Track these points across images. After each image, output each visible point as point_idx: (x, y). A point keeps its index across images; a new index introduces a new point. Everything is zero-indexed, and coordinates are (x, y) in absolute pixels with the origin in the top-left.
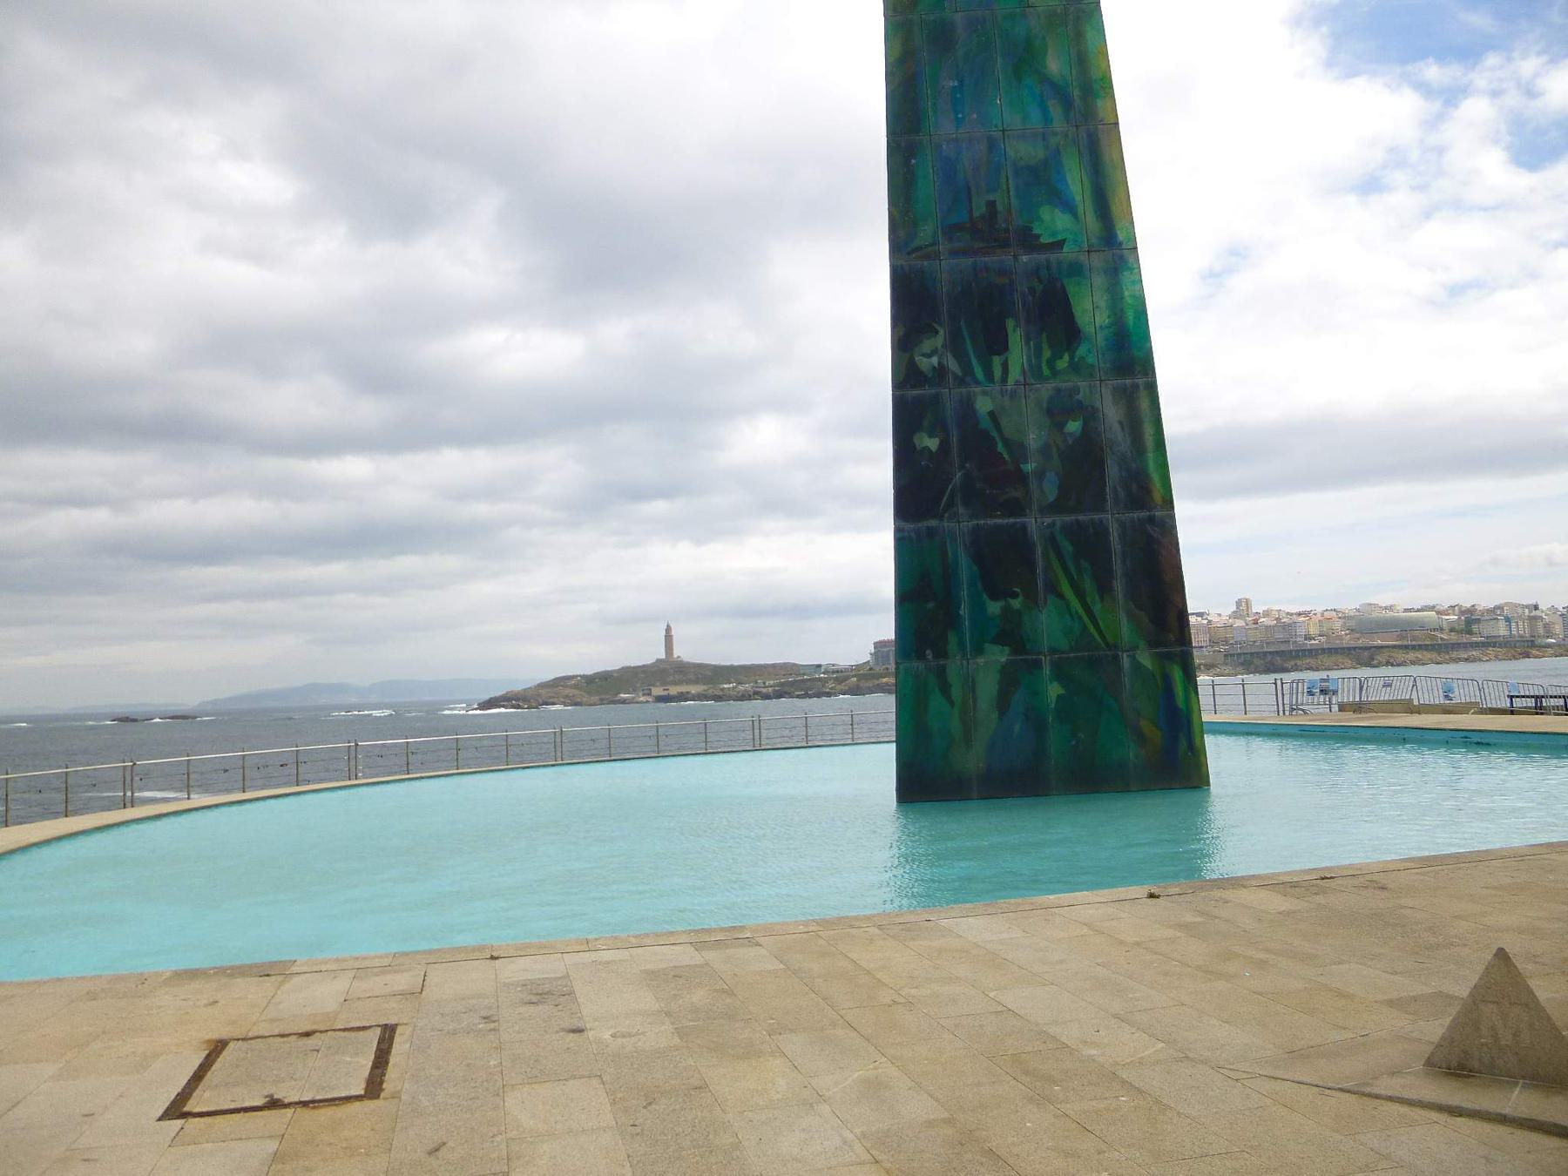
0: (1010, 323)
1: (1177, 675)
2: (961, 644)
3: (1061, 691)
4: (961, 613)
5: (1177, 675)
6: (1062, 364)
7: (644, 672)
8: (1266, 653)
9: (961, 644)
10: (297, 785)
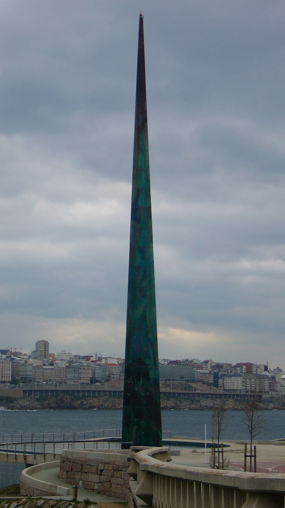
0: (141, 377)
8: (57, 391)
10: (170, 438)
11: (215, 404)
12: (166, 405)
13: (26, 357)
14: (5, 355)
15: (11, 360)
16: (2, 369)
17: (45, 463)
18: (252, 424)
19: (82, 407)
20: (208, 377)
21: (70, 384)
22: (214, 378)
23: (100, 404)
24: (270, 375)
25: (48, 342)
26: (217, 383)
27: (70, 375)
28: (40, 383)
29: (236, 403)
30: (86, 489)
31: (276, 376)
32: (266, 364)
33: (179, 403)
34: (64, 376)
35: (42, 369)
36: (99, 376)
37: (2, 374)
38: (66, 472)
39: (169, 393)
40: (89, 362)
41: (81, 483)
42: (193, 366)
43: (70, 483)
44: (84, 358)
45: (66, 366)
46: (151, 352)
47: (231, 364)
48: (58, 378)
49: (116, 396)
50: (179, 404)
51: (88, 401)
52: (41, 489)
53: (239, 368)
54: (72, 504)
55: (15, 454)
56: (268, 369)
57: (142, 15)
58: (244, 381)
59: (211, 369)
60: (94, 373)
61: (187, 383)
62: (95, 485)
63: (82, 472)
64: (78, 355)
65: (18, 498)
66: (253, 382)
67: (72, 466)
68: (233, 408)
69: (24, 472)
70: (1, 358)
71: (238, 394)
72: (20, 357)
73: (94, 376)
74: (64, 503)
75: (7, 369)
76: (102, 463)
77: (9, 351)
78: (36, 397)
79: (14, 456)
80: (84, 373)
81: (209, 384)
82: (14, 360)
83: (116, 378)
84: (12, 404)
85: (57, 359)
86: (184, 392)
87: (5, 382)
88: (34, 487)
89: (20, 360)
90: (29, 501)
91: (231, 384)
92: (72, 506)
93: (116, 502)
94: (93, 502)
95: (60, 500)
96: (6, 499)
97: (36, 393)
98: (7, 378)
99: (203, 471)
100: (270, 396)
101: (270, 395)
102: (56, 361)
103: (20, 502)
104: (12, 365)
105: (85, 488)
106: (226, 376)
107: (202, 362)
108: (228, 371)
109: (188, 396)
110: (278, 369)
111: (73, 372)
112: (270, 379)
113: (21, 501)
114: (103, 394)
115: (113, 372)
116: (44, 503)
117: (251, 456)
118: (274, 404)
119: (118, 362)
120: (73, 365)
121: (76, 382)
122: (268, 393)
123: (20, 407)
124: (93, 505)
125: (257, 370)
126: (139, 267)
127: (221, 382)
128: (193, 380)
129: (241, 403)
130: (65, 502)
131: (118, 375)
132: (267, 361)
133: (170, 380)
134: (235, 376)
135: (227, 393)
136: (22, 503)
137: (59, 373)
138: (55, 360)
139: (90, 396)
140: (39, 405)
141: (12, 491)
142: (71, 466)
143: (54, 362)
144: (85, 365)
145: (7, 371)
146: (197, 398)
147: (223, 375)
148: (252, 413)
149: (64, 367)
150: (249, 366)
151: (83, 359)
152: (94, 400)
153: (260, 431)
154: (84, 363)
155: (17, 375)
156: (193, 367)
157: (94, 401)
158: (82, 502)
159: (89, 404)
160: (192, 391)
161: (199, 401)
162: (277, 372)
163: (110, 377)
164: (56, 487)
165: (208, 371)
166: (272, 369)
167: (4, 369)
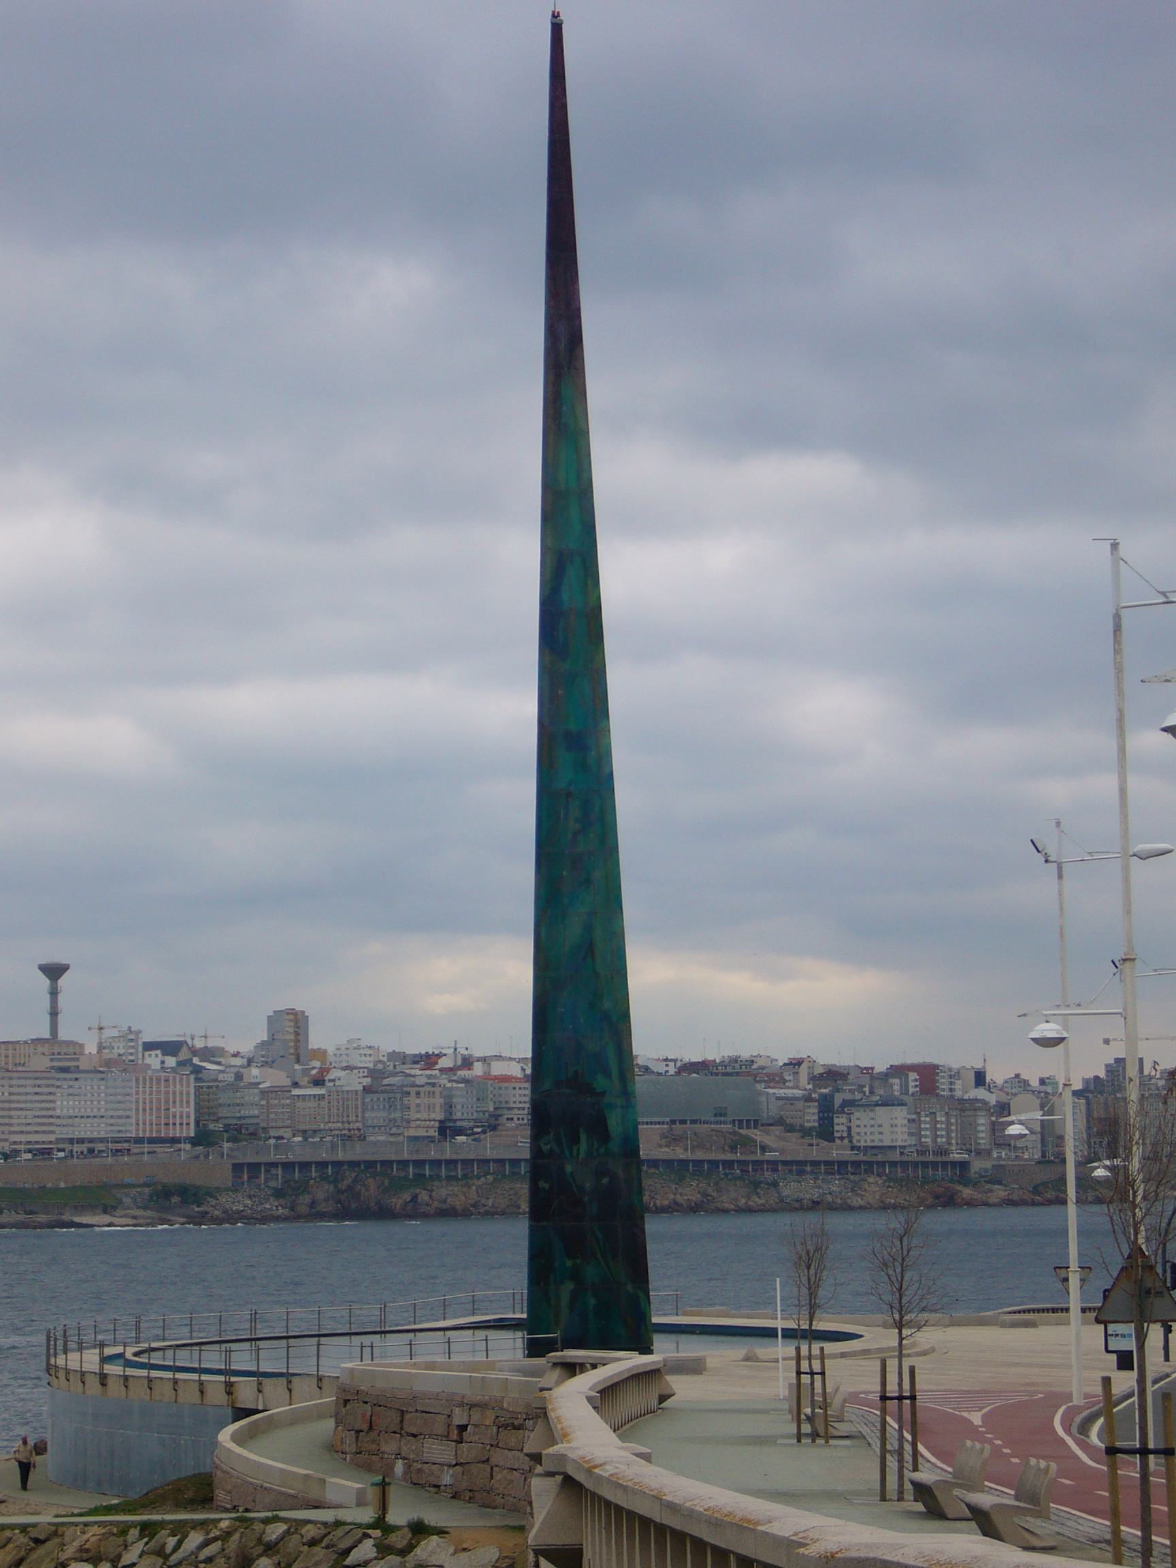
0: (581, 1130)
1: (641, 1295)
3: (595, 1302)
5: (641, 1295)
6: (602, 1150)
8: (338, 1164)
11: (824, 1193)
12: (674, 1200)
13: (238, 1061)
14: (174, 1058)
15: (192, 1072)
16: (167, 1102)
17: (291, 1405)
18: (901, 1299)
19: (413, 1212)
20: (800, 1111)
21: (375, 1143)
22: (819, 1112)
23: (470, 1201)
24: (992, 1099)
25: (306, 1014)
26: (831, 1129)
27: (377, 1116)
28: (286, 1141)
29: (889, 1187)
30: (415, 1484)
31: (1011, 1102)
32: (979, 1065)
33: (714, 1191)
34: (357, 1116)
35: (287, 1098)
36: (465, 1114)
37: (167, 1117)
38: (353, 1432)
39: (684, 1163)
40: (433, 1072)
41: (399, 1467)
42: (756, 1077)
43: (368, 1468)
44: (416, 1059)
45: (362, 1088)
46: (611, 1053)
47: (872, 1069)
48: (339, 1125)
49: (520, 1173)
50: (715, 1194)
51: (434, 1194)
52: (277, 1488)
53: (897, 1081)
54: (373, 1536)
55: (200, 1380)
56: (988, 1079)
57: (558, 13)
58: (913, 1120)
59: (810, 1086)
60: (449, 1107)
61: (737, 1129)
62: (443, 1471)
63: (402, 1436)
64: (399, 1053)
65: (207, 1519)
66: (942, 1122)
67: (371, 1416)
68: (881, 1204)
69: (225, 1436)
70: (162, 1068)
71: (896, 1160)
72: (219, 1063)
73: (451, 1114)
74: (349, 1532)
75: (181, 1101)
76: (462, 1405)
77: (185, 1045)
78: (272, 1184)
79: (197, 1384)
80: (418, 1105)
81: (806, 1132)
82: (201, 1072)
83: (518, 1119)
84: (198, 1206)
85: (334, 1065)
86: (729, 1156)
87: (174, 1141)
88: (256, 1481)
89: (220, 1071)
90: (239, 1527)
91: (872, 1130)
92: (372, 1540)
93: (507, 1526)
94: (435, 1527)
95: (334, 1523)
96: (171, 1522)
97: (274, 1171)
98: (181, 1129)
99: (706, 1507)
100: (995, 1163)
101: (995, 1159)
102: (330, 1072)
103: (215, 1530)
104: (195, 1086)
105: (412, 1483)
106: (859, 1105)
107: (782, 1064)
108: (864, 1089)
109: (742, 1171)
110: (1017, 1080)
111: (384, 1107)
112: (992, 1111)
113: (216, 1527)
114: (478, 1169)
115: (507, 1102)
116: (287, 1533)
117: (900, 1398)
118: (1008, 1188)
119: (523, 1070)
120: (386, 1082)
121: (394, 1134)
122: (989, 1153)
123: (223, 1215)
124: (435, 1537)
125: (951, 1083)
126: (569, 795)
127: (843, 1124)
128: (756, 1121)
129: (905, 1189)
130: (352, 1529)
131: (523, 1109)
132: (984, 1055)
133: (683, 1122)
134: (885, 1104)
135: (861, 1157)
136: (218, 1533)
137: (341, 1108)
138: (328, 1070)
139: (438, 1177)
140: (283, 1208)
141: (190, 1494)
142: (369, 1414)
143: (325, 1074)
144: (422, 1081)
145: (182, 1106)
146: (769, 1176)
147: (846, 1103)
148: (902, 1267)
149: (357, 1091)
150: (928, 1074)
151: (416, 1063)
152: (450, 1188)
153: (926, 1321)
154: (420, 1074)
155: (211, 1117)
156: (755, 1079)
157: (451, 1193)
158: (403, 1527)
159: (436, 1203)
160: (752, 1153)
161: (775, 1184)
162: (1014, 1091)
163: (500, 1116)
164: (325, 1480)
165: (801, 1092)
166: (1000, 1081)
167: (171, 1099)
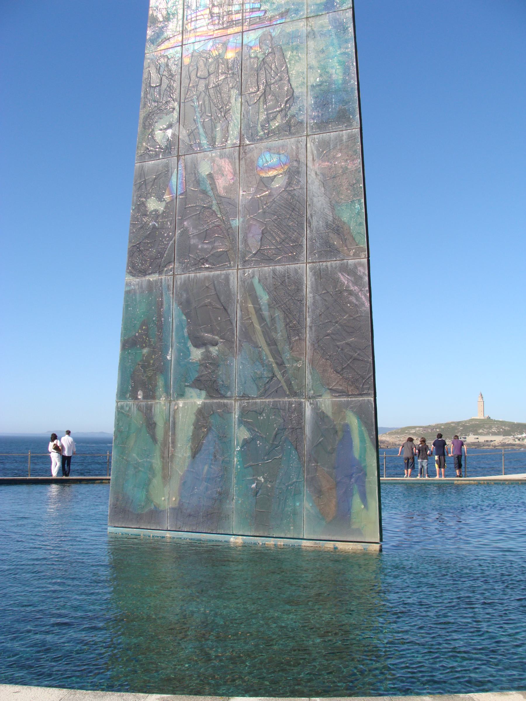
2: (167, 387)
4: (169, 358)
7: (463, 426)
9: (167, 387)
